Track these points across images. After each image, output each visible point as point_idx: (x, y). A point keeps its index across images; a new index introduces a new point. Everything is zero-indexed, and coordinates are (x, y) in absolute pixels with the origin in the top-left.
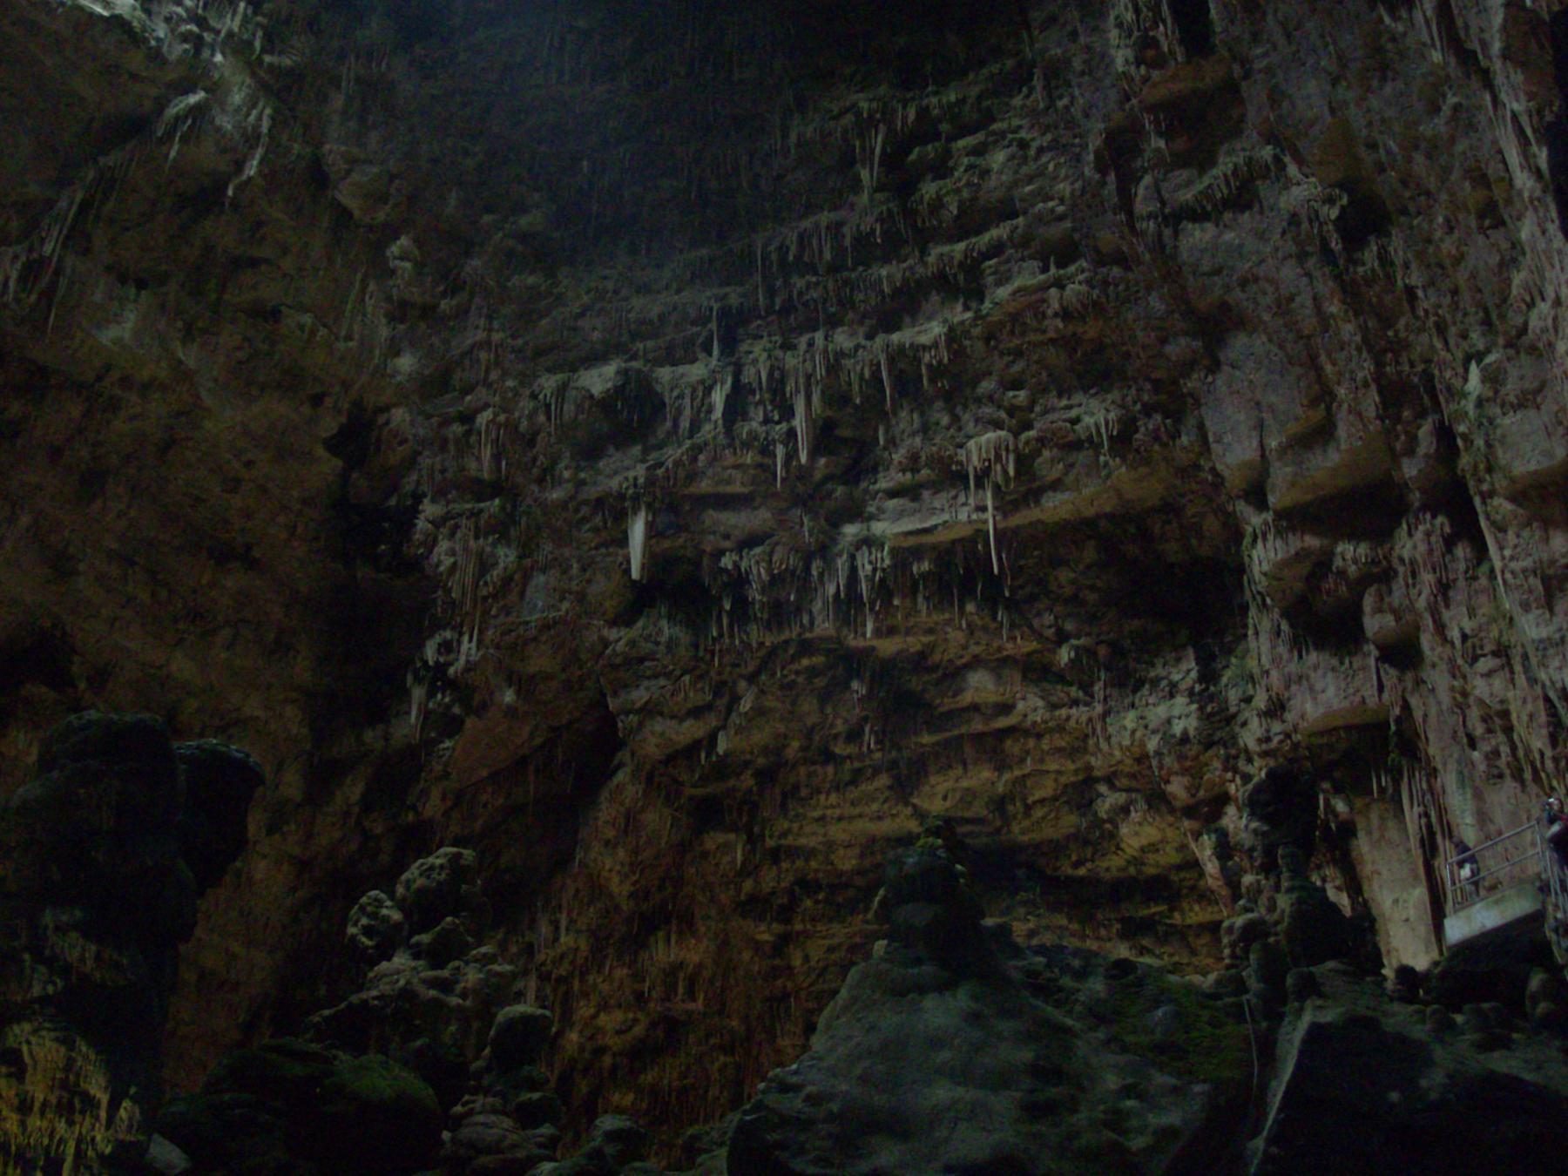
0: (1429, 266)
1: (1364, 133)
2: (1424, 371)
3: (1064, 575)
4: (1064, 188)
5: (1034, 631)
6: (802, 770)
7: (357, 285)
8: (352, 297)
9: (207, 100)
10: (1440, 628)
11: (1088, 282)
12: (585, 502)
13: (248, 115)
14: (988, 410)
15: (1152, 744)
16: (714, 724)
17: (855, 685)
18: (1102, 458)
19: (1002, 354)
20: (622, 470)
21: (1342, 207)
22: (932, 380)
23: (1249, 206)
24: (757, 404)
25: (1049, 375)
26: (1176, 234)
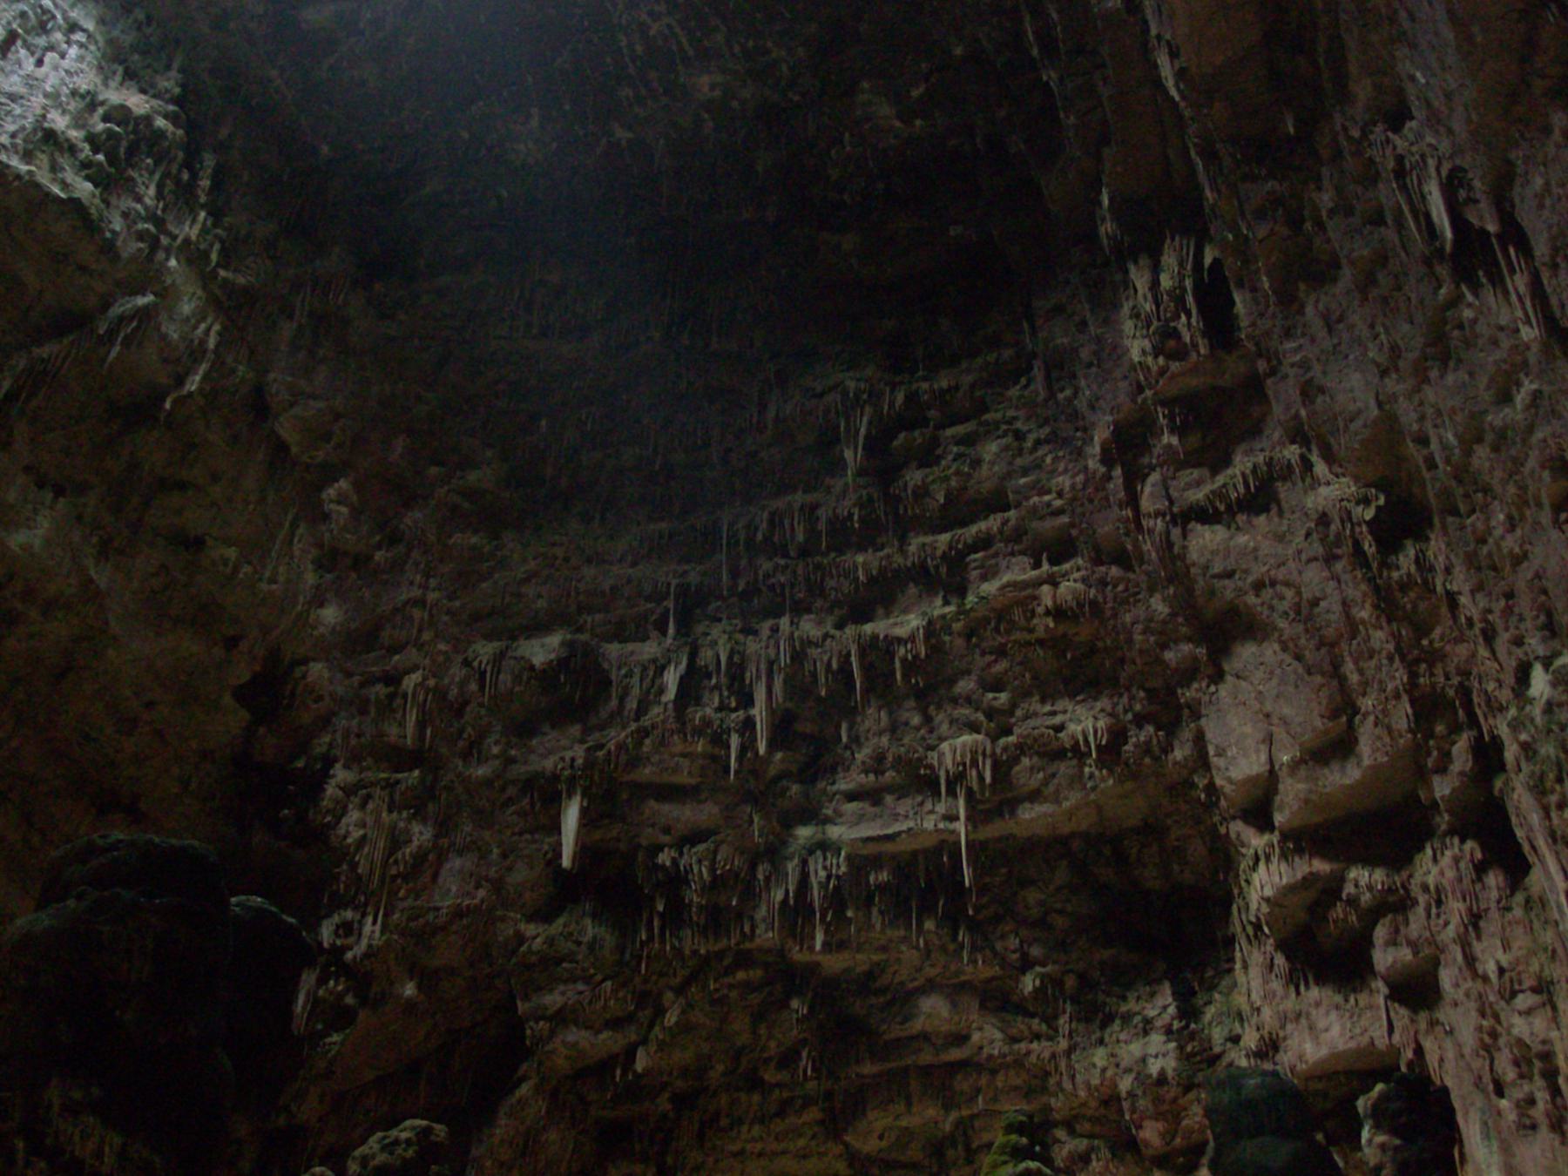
0: (1479, 569)
1: (1415, 427)
2: (1461, 684)
3: (1032, 896)
4: (1064, 481)
5: (995, 954)
6: (724, 1099)
7: (287, 525)
8: (281, 536)
9: (155, 305)
10: (1470, 960)
11: (1084, 580)
12: (513, 782)
13: (195, 328)
14: (964, 712)
15: (1125, 1084)
16: (633, 1037)
17: (795, 1004)
18: (1087, 770)
19: (983, 653)
20: (560, 750)
21: (1378, 508)
22: (905, 676)
23: (1267, 510)
24: (712, 689)
25: (1034, 678)
26: (1185, 536)
